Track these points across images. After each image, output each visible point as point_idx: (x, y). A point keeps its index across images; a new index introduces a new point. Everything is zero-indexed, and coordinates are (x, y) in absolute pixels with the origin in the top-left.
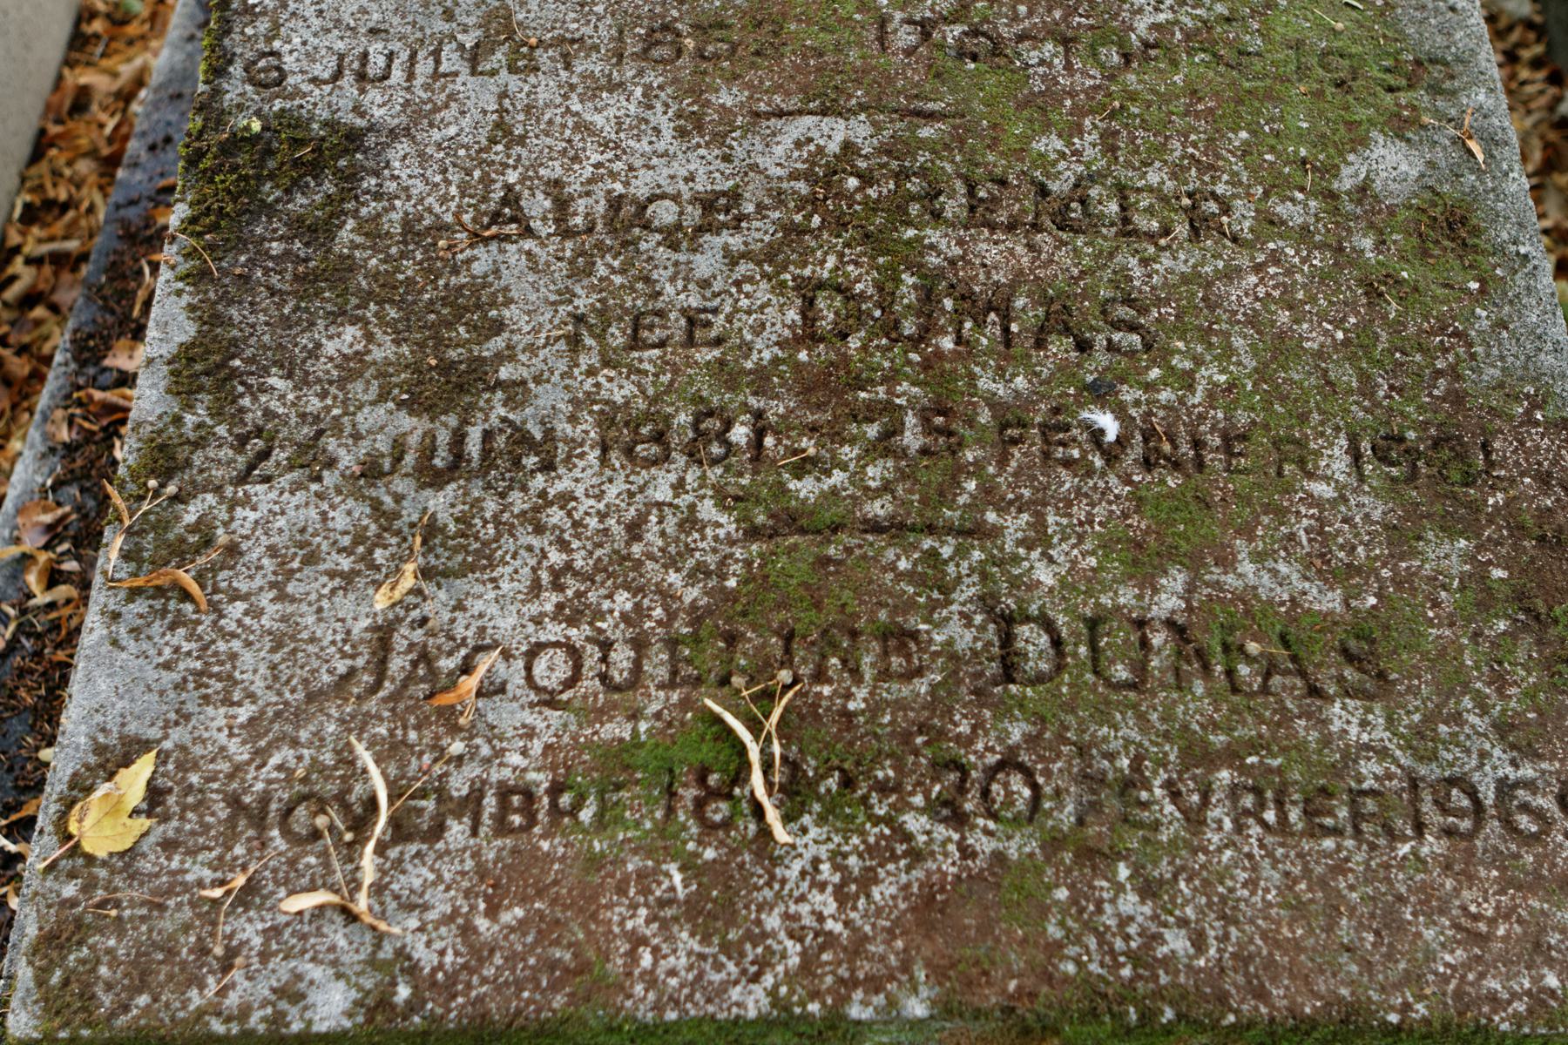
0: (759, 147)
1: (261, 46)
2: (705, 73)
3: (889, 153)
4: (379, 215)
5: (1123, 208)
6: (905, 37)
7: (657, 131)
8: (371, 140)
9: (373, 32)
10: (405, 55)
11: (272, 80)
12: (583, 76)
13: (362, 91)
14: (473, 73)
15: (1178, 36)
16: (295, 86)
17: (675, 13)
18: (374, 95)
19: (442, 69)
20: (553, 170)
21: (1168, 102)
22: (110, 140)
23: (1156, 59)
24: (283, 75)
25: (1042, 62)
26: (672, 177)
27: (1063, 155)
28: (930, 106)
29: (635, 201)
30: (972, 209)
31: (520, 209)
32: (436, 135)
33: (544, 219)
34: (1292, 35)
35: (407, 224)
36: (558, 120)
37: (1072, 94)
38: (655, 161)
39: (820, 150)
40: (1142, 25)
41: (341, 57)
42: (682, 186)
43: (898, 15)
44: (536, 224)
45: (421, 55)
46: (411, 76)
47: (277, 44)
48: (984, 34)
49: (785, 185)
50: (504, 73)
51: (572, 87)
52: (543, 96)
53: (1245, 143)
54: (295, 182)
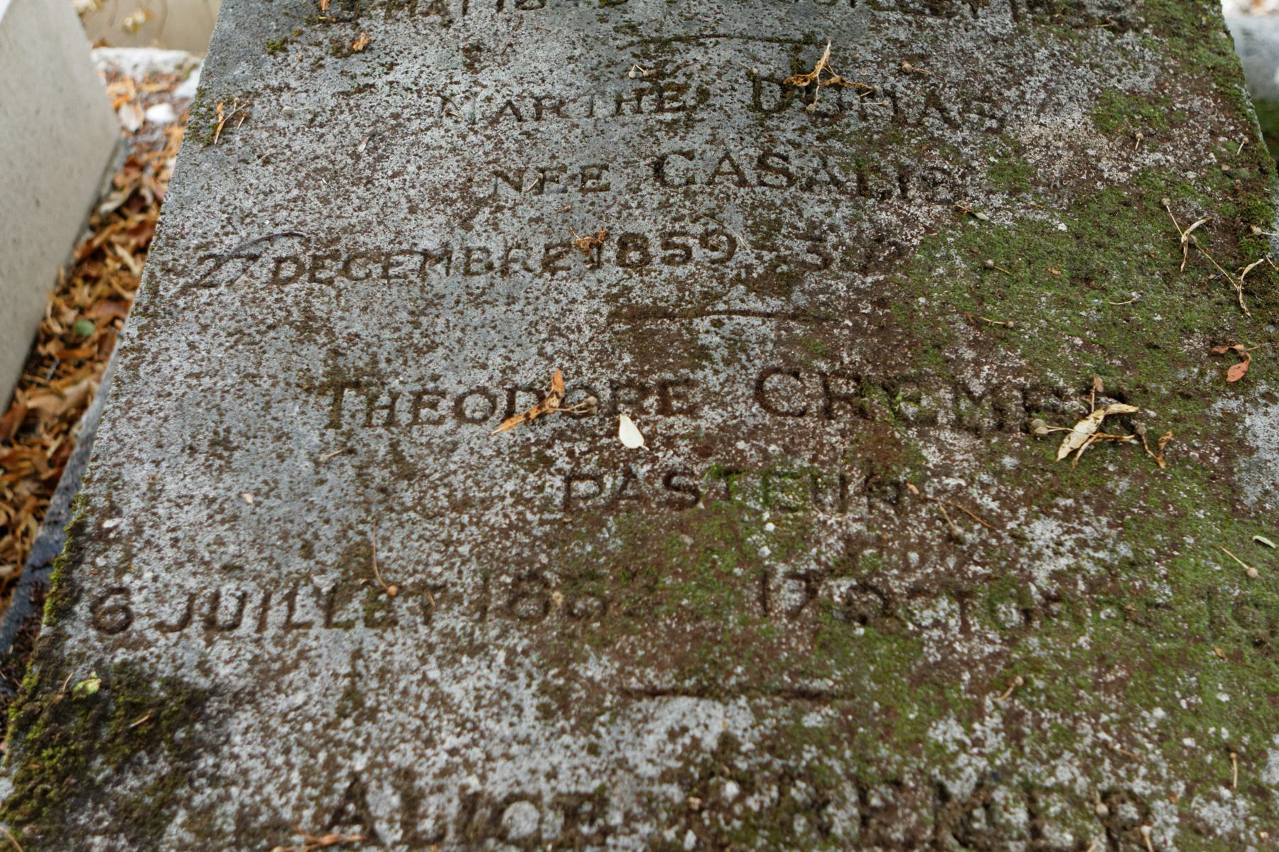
0: (629, 736)
1: (110, 580)
2: (573, 636)
3: (772, 750)
4: (212, 806)
5: (1032, 815)
6: (789, 595)
7: (519, 709)
8: (213, 706)
9: (228, 569)
10: (257, 599)
11: (116, 624)
12: (444, 635)
13: (210, 643)
14: (328, 624)
15: (1082, 586)
16: (141, 634)
17: (544, 558)
18: (222, 648)
19: (296, 618)
20: (403, 756)
21: (1074, 673)
22: (51, 463)
23: (1059, 615)
24: (130, 618)
25: (936, 623)
26: (533, 772)
27: (962, 746)
28: (817, 684)
29: (490, 802)
30: (864, 821)
31: (365, 806)
32: (283, 703)
33: (391, 821)
34: (1203, 582)
35: (242, 819)
36: (414, 689)
37: (970, 665)
38: (515, 749)
39: (696, 742)
40: (1041, 573)
41: (192, 598)
42: (543, 785)
43: (782, 568)
44: (381, 827)
45: (275, 599)
46: (262, 626)
47: (127, 579)
48: (874, 589)
49: (656, 789)
50: (360, 626)
51: (431, 648)
52: (399, 658)
53: (1161, 723)
54: (127, 759)
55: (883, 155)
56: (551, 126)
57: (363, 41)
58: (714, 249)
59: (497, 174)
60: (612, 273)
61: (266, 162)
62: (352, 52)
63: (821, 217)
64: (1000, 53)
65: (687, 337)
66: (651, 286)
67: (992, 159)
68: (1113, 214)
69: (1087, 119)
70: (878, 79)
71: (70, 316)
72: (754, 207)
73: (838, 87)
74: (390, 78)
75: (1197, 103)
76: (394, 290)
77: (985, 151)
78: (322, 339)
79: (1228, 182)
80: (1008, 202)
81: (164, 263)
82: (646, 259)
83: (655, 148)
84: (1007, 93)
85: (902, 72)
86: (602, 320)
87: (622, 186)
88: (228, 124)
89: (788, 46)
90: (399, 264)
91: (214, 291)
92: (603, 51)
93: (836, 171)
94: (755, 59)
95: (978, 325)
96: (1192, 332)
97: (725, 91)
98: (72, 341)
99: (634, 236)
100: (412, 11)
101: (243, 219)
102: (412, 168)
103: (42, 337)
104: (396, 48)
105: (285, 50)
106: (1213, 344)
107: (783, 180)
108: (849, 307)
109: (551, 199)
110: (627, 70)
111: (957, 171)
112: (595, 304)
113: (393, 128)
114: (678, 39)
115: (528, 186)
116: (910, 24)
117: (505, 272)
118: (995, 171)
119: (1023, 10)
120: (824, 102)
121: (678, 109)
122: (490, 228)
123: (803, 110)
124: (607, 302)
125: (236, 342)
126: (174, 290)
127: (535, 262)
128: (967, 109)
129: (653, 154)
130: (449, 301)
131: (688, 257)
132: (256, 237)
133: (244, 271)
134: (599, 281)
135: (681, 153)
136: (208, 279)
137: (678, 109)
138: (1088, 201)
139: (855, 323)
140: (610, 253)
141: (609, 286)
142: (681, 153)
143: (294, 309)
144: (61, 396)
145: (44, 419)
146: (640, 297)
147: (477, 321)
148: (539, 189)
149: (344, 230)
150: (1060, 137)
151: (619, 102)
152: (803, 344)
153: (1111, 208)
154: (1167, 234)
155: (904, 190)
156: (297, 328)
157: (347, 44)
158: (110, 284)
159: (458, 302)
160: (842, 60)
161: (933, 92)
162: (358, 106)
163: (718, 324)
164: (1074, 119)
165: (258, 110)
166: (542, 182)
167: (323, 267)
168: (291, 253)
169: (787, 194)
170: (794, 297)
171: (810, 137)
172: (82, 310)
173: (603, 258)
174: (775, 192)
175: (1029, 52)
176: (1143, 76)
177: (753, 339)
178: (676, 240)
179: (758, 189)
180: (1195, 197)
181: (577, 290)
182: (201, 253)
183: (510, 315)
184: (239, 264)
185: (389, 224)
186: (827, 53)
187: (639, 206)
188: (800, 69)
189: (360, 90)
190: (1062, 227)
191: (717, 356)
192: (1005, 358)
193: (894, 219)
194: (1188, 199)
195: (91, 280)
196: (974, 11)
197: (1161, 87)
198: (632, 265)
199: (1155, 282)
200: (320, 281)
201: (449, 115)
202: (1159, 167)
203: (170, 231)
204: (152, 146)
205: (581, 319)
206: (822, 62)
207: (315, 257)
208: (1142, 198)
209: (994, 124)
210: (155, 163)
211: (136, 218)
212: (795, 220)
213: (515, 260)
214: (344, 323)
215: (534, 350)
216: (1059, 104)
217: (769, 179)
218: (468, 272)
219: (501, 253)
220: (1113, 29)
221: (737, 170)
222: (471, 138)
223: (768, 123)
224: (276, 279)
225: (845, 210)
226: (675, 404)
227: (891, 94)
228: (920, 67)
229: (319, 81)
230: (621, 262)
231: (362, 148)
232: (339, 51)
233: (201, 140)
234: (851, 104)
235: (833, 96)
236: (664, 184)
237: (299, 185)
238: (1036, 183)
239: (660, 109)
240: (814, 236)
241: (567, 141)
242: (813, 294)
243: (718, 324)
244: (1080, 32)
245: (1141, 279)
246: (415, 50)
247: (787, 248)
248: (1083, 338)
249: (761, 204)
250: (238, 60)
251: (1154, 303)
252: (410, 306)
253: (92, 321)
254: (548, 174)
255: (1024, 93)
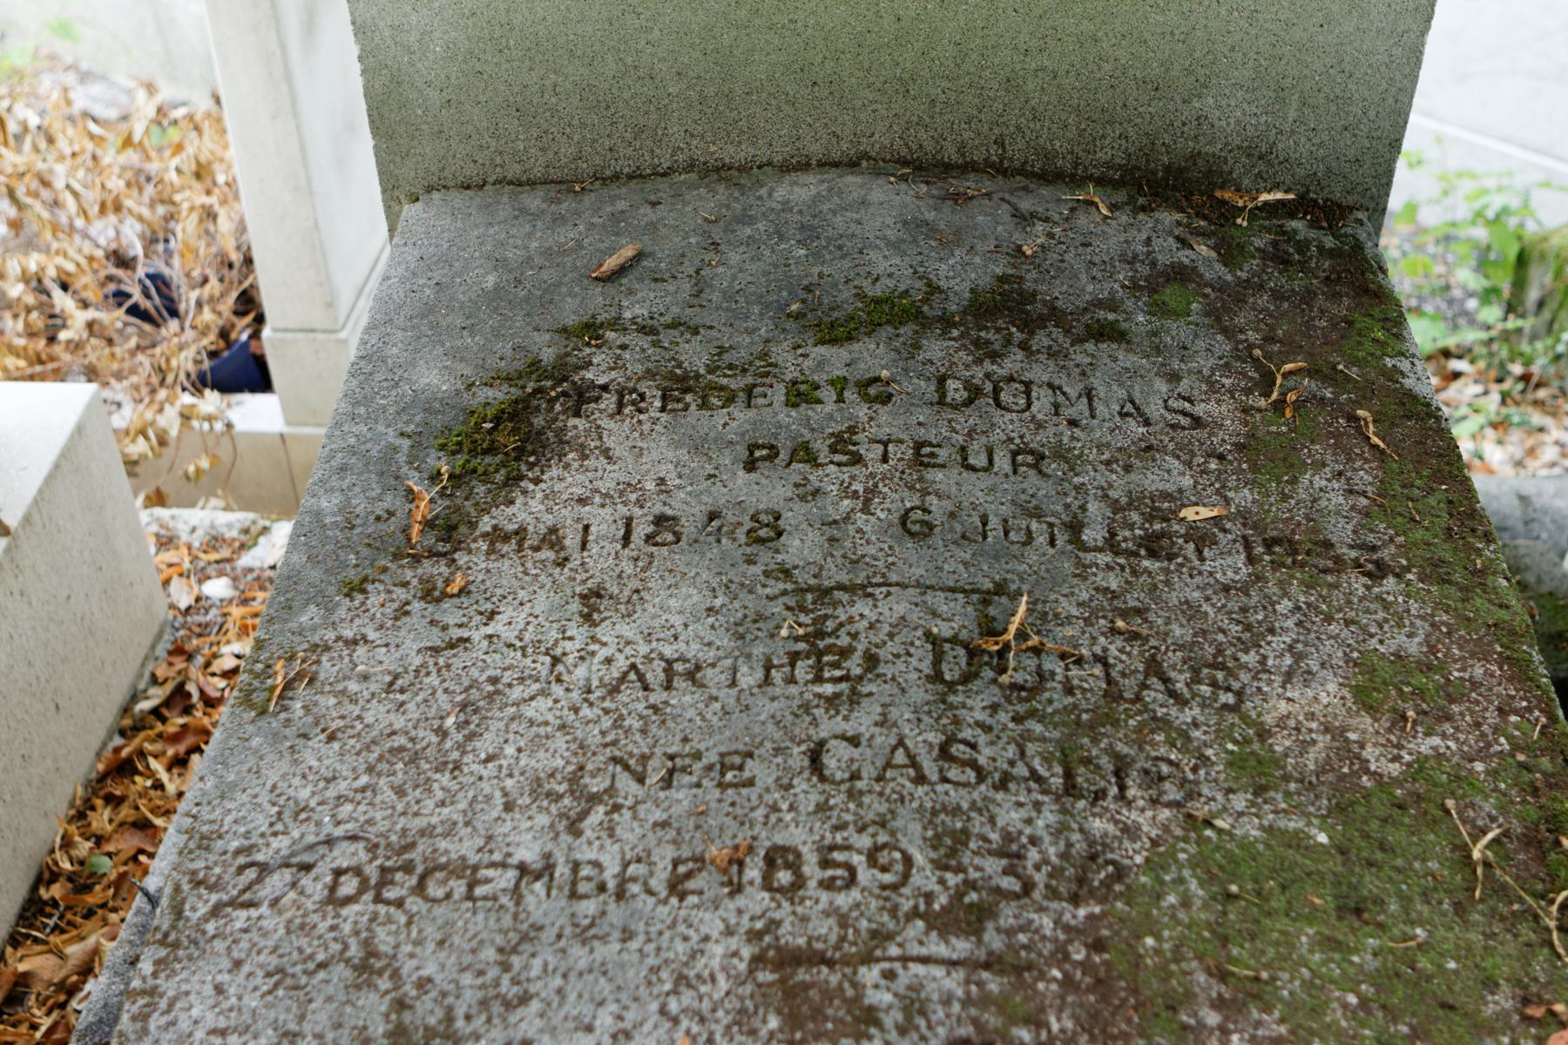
55: (1095, 741)
56: (684, 698)
57: (459, 582)
58: (884, 869)
59: (615, 760)
60: (756, 900)
61: (332, 738)
62: (445, 595)
63: (1020, 826)
64: (1233, 605)
65: (850, 992)
66: (805, 919)
67: (1230, 746)
68: (1385, 820)
69: (1345, 692)
70: (1085, 640)
71: (84, 847)
72: (934, 813)
73: (1037, 651)
74: (489, 630)
75: (1478, 671)
76: (480, 917)
77: (1222, 735)
78: (384, 984)
79: (1526, 777)
80: (1253, 804)
81: (194, 873)
82: (799, 882)
83: (812, 731)
84: (1244, 658)
85: (1114, 631)
86: (742, 967)
87: (770, 780)
88: (288, 686)
89: (975, 597)
90: (488, 881)
91: (253, 913)
92: (750, 601)
93: (1037, 763)
94: (935, 614)
95: (1223, 976)
96: (1497, 985)
97: (897, 656)
98: (82, 882)
99: (785, 849)
100: (520, 545)
101: (297, 814)
102: (510, 750)
103: (46, 875)
104: (499, 592)
105: (364, 591)
106: (1526, 1001)
107: (971, 775)
108: (1057, 951)
109: (682, 796)
110: (779, 627)
111: (1187, 762)
112: (734, 943)
113: (490, 697)
114: (841, 587)
115: (653, 779)
116: (1123, 568)
117: (620, 895)
118: (1234, 762)
119: (1259, 549)
120: (1019, 671)
121: (840, 679)
122: (604, 834)
123: (995, 681)
124: (749, 941)
125: (276, 986)
126: (203, 910)
127: (659, 883)
128: (1196, 679)
129: (809, 738)
130: (549, 935)
131: (852, 880)
132: (311, 839)
133: (294, 885)
134: (740, 912)
135: (844, 737)
136: (247, 896)
137: (840, 679)
138: (1352, 803)
139: (1065, 974)
140: (753, 873)
141: (752, 919)
142: (844, 737)
143: (352, 942)
144: (62, 956)
145: (37, 988)
146: (791, 936)
147: (582, 964)
148: (667, 782)
149: (422, 833)
150: (1311, 716)
151: (768, 667)
152: (1000, 1004)
153: (1382, 811)
154: (1455, 848)
155: (1122, 788)
156: (355, 968)
157: (440, 584)
158: (137, 808)
159: (559, 936)
160: (1042, 617)
161: (1153, 656)
162: (448, 666)
163: (889, 975)
164: (1329, 692)
165: (327, 668)
166: (671, 772)
167: (392, 882)
168: (354, 862)
169: (976, 795)
170: (986, 937)
171: (1003, 717)
172: (100, 840)
173: (745, 879)
174: (962, 792)
175: (1269, 604)
176: (1410, 636)
177: (935, 997)
178: (838, 856)
179: (940, 788)
180: (1486, 797)
181: (711, 923)
182: (241, 860)
183: (625, 956)
184: (287, 875)
185: (479, 825)
186: (1022, 608)
187: (792, 808)
188: (991, 629)
189: (452, 645)
190: (1323, 838)
191: (888, 1021)
192: (1258, 1024)
193: (1111, 828)
194: (1478, 800)
195: (114, 801)
196: (1199, 552)
197: (1432, 649)
198: (780, 890)
199: (1444, 914)
200: (388, 903)
201: (559, 680)
202: (1439, 756)
203: (205, 828)
204: (203, 630)
205: (716, 963)
206: (1017, 619)
207: (383, 870)
208: (1423, 798)
209: (1230, 698)
210: (206, 651)
211: (177, 721)
212: (987, 830)
213: (634, 880)
214: (414, 963)
215: (654, 1006)
216: (1309, 673)
217: (953, 774)
218: (574, 895)
219: (617, 869)
220: (1369, 574)
221: (913, 762)
222: (586, 712)
223: (951, 698)
224: (333, 899)
225: (1049, 817)
226: (827, 675)
227: (1102, 660)
228: (1136, 624)
229: (403, 632)
230: (768, 884)
231: (450, 721)
232: (430, 594)
233: (252, 706)
234: (1053, 674)
235: (1031, 662)
236: (823, 779)
237: (370, 770)
238: (1287, 778)
239: (818, 679)
240: (1010, 852)
241: (704, 719)
242: (1010, 932)
243: (889, 975)
244: (1329, 578)
245: (1425, 909)
246: (522, 594)
247: (978, 868)
248: (1358, 994)
249: (944, 809)
250: (308, 602)
251: (1443, 943)
252: (499, 940)
253: (109, 855)
254: (679, 762)
255: (1265, 658)
